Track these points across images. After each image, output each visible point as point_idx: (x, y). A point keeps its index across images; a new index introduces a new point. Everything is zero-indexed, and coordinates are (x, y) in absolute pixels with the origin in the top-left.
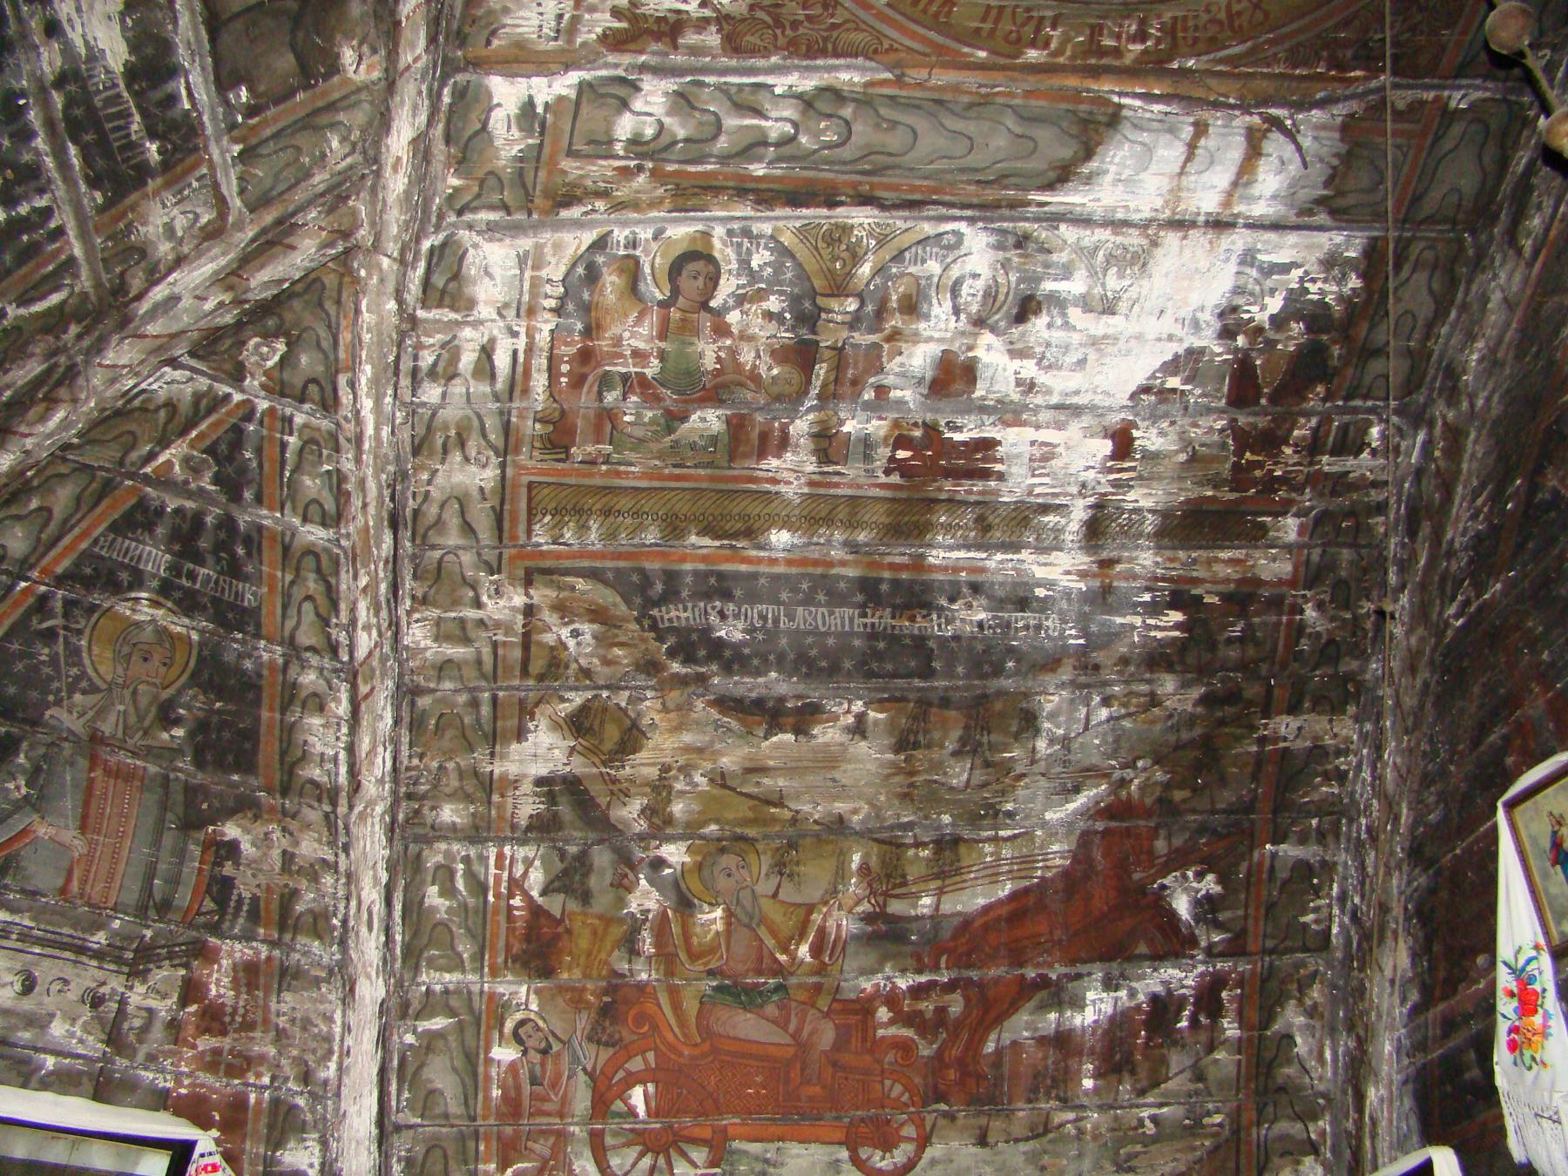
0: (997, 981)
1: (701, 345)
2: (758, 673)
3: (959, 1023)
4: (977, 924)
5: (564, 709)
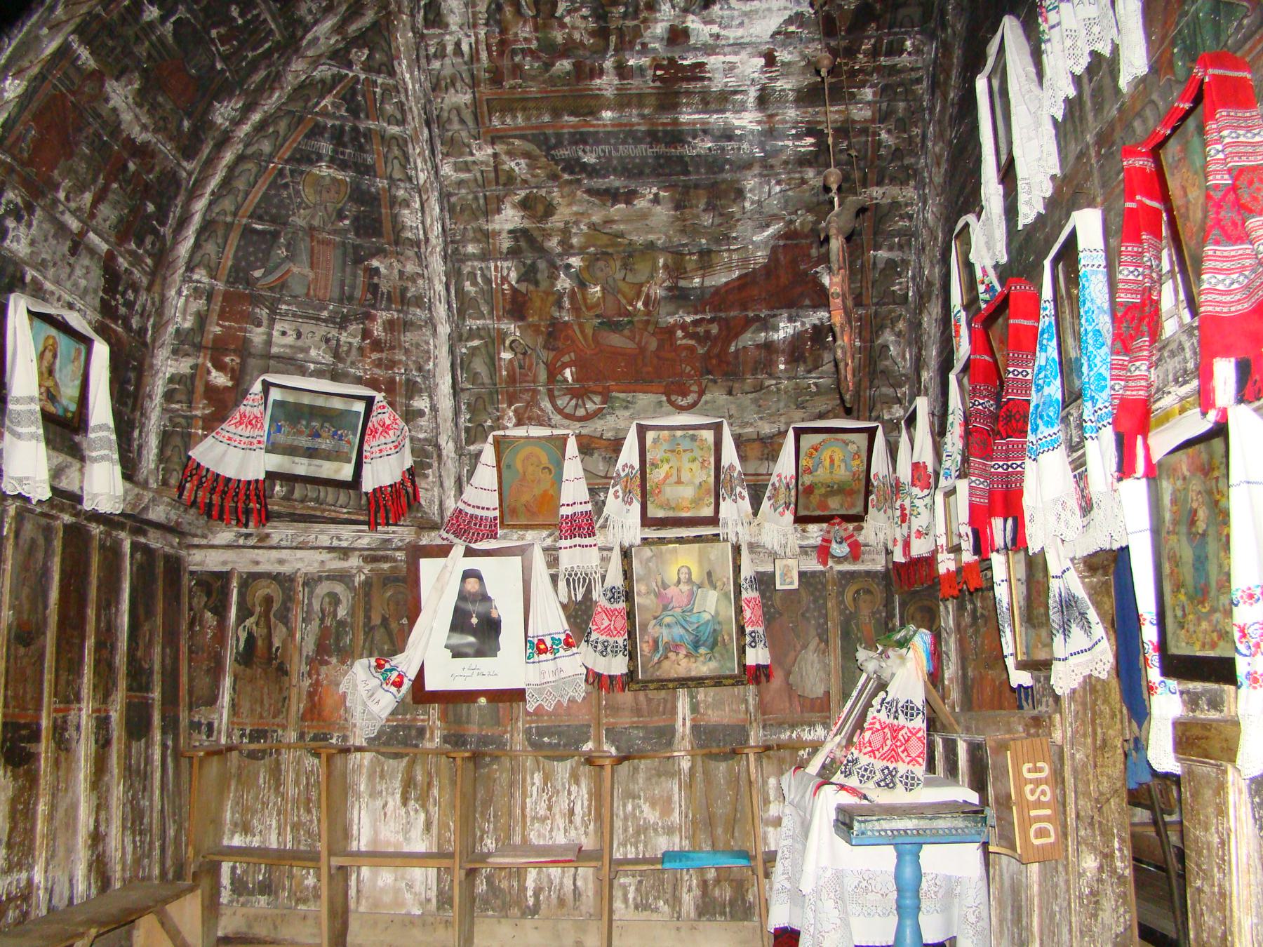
0: (735, 317)
1: (554, 33)
2: (604, 177)
3: (716, 338)
4: (723, 291)
5: (517, 198)
